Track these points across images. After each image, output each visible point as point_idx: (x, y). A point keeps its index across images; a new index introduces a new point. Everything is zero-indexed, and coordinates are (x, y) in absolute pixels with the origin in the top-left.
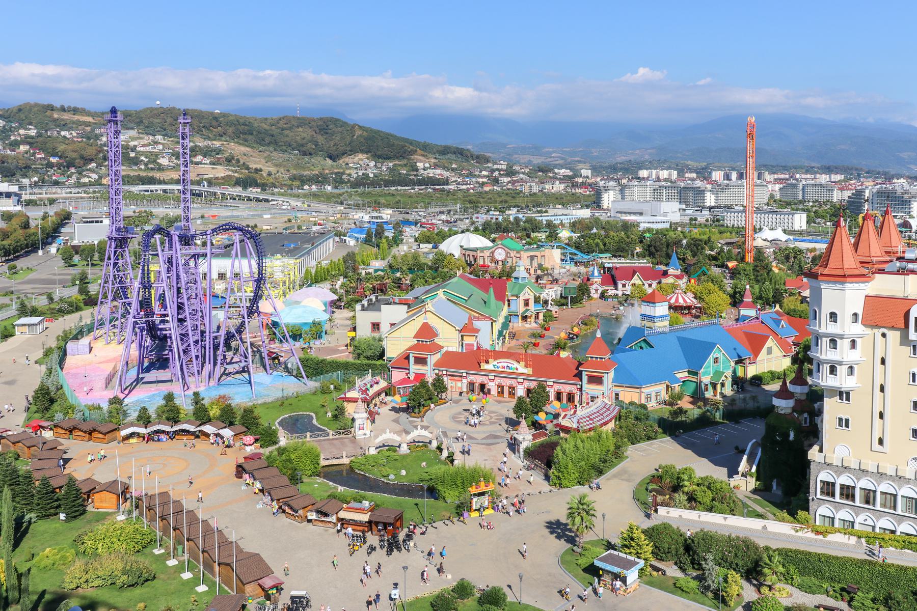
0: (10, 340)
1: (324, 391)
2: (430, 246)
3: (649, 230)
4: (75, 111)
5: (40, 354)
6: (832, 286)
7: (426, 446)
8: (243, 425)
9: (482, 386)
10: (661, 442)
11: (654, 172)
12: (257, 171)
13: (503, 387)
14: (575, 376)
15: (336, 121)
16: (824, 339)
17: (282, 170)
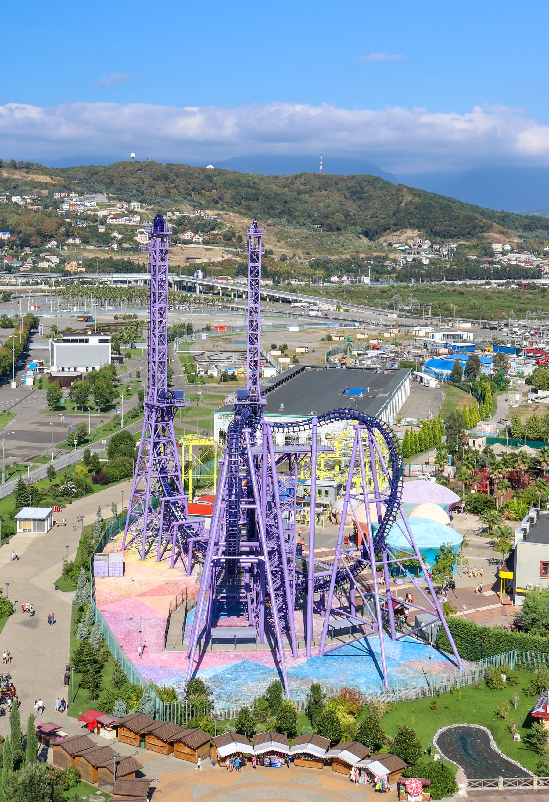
0: (13, 540)
1: (490, 683)
4: (28, 167)
5: (56, 571)
17: (299, 252)
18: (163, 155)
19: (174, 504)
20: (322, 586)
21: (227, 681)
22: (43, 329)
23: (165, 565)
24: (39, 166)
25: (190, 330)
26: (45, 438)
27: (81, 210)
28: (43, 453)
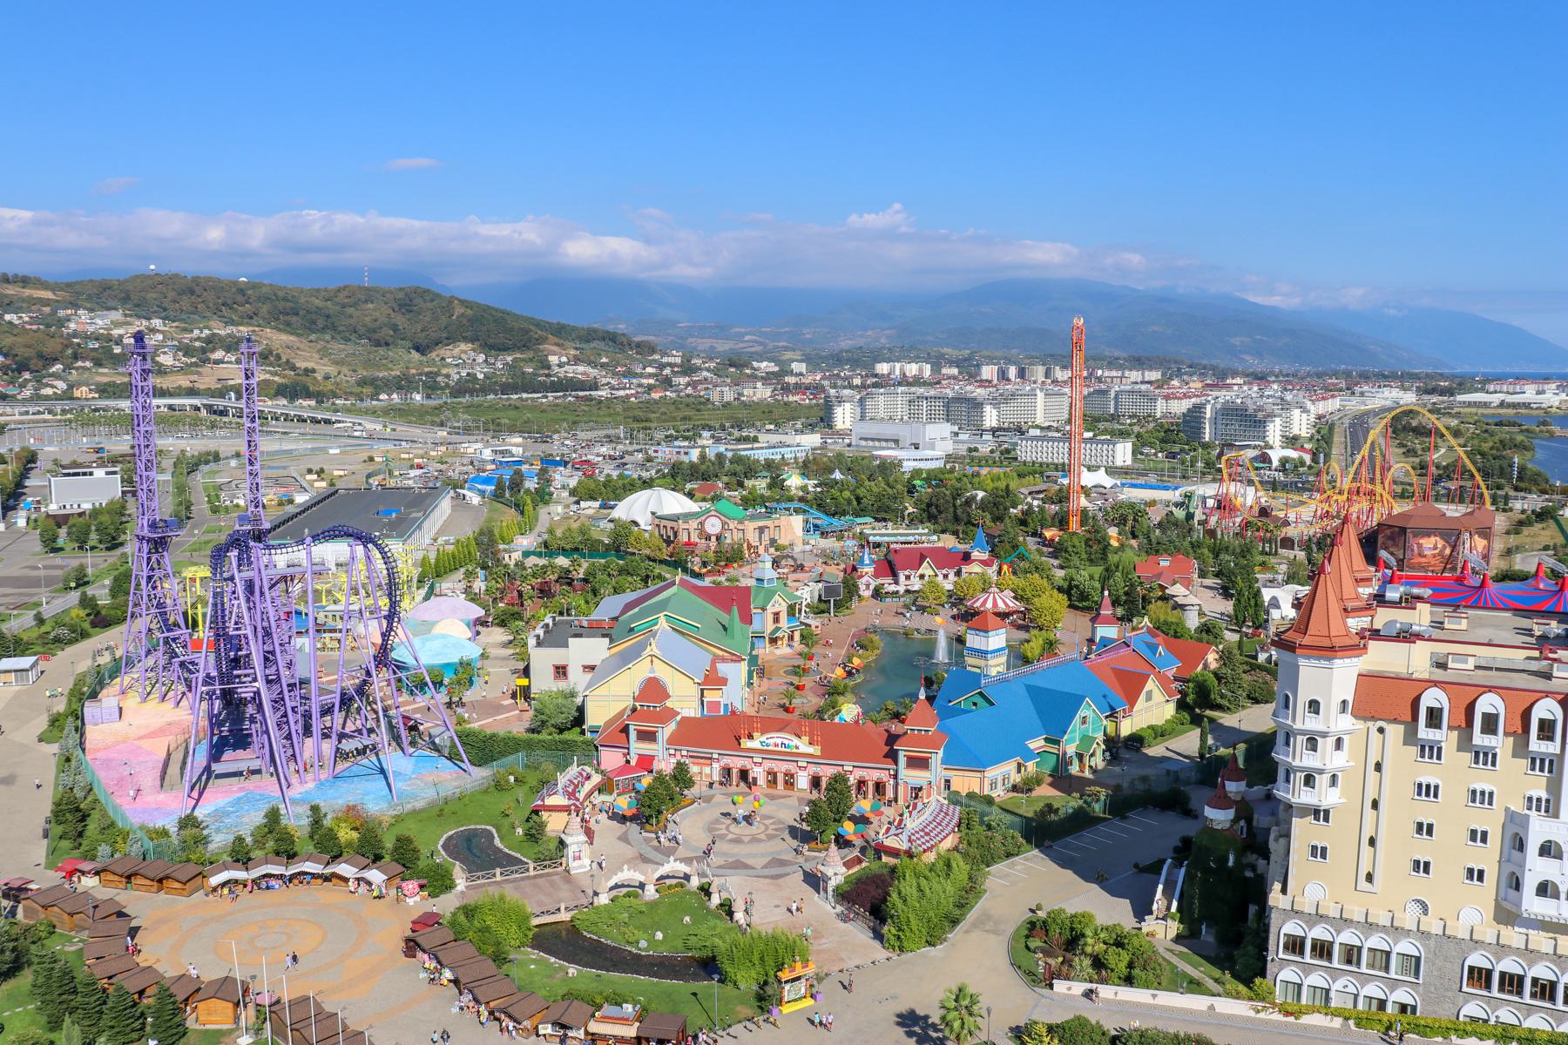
1: (499, 786)
2: (596, 504)
3: (916, 473)
4: (25, 281)
5: (42, 723)
6: (1314, 662)
7: (682, 886)
8: (397, 861)
9: (744, 774)
10: (1026, 859)
11: (898, 366)
12: (307, 372)
13: (775, 775)
14: (886, 756)
15: (424, 293)
16: (1299, 738)
17: (345, 370)
18: (188, 268)
19: (174, 640)
20: (327, 711)
21: (227, 814)
22: (43, 462)
23: (168, 705)
24: (39, 280)
25: (216, 457)
26: (35, 583)
27: (91, 329)
28: (35, 599)
